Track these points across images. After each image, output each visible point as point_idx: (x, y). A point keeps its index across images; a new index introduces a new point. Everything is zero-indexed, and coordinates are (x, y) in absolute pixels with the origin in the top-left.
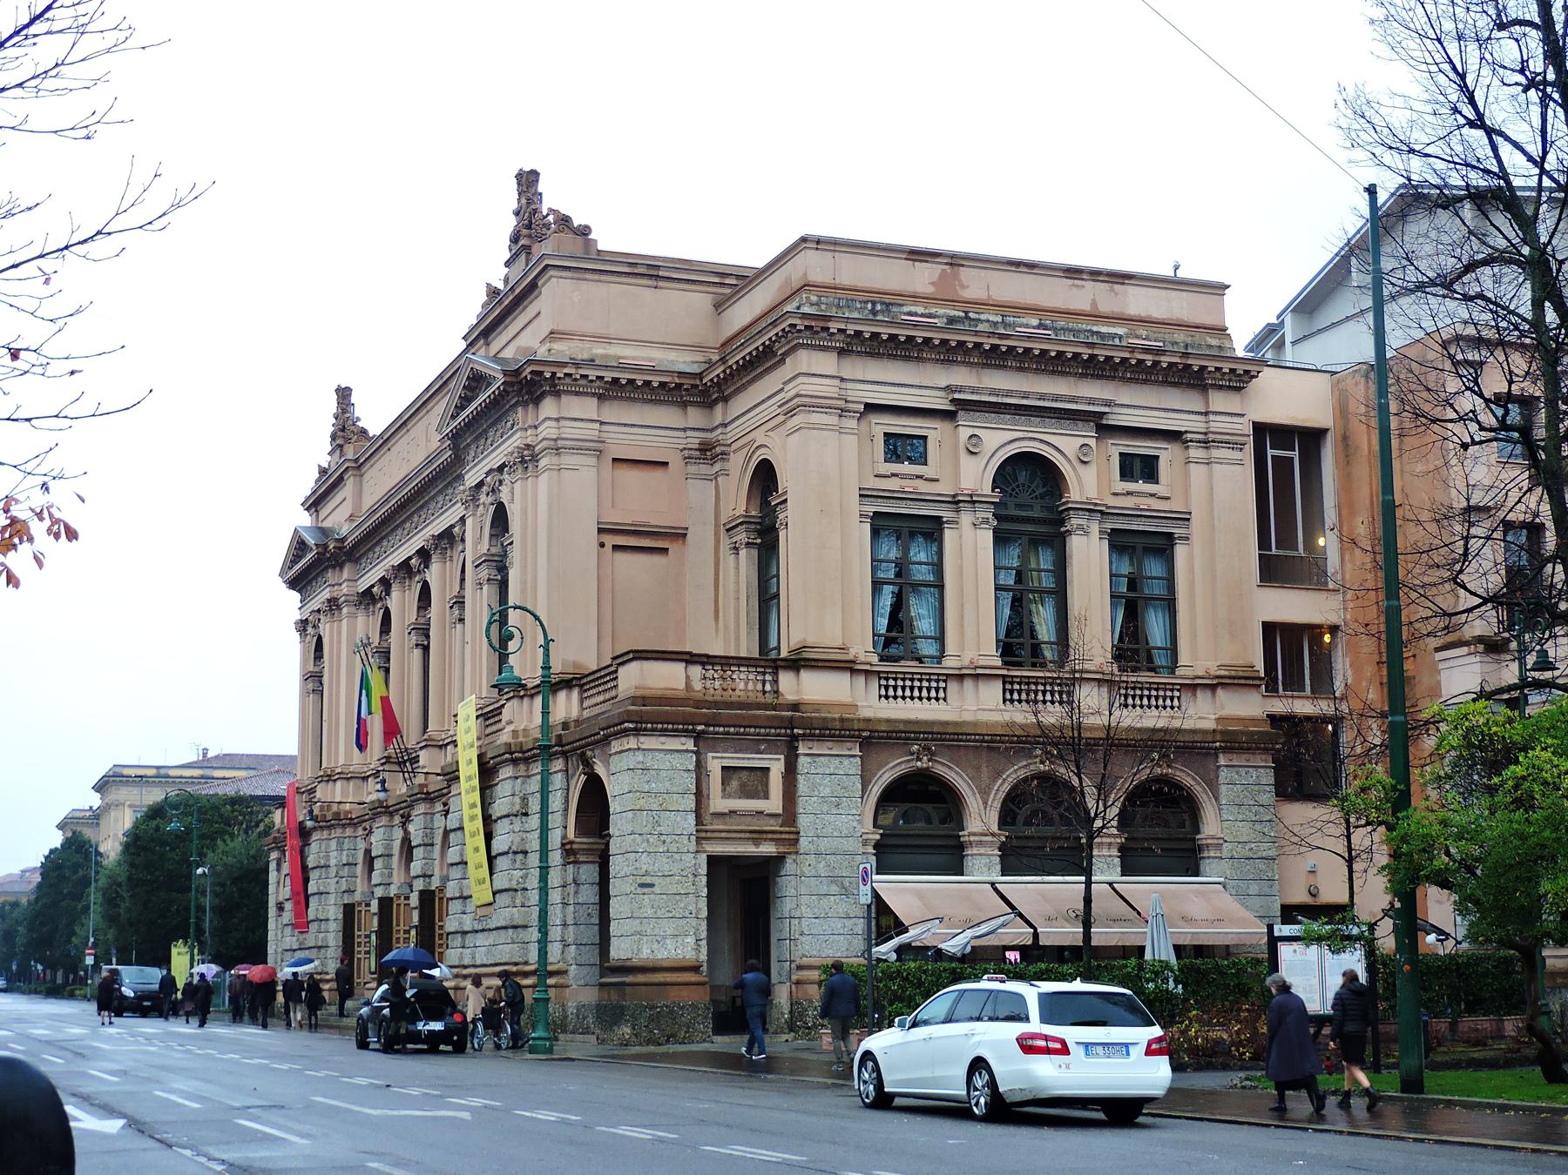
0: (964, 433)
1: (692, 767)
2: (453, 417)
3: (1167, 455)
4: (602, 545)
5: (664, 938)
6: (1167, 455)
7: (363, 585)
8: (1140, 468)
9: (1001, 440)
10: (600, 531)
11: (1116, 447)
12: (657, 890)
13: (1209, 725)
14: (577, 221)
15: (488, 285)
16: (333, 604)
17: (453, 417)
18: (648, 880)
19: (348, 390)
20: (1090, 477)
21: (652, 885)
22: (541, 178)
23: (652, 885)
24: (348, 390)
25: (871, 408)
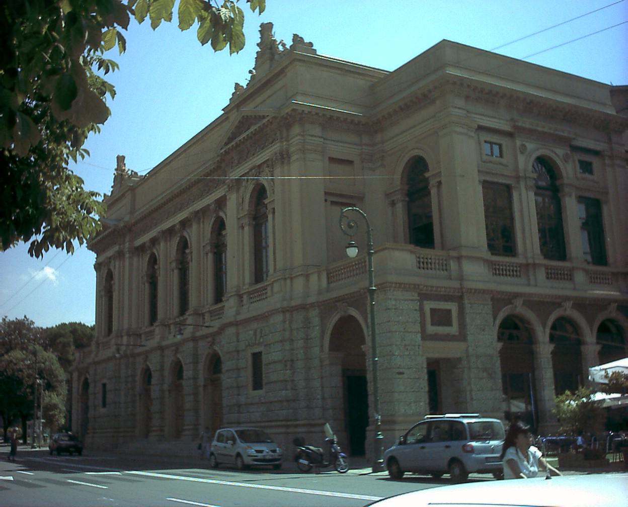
0: (518, 143)
1: (417, 308)
2: (226, 144)
3: (596, 162)
4: (326, 201)
5: (410, 403)
6: (596, 162)
7: (138, 242)
8: (586, 167)
9: (534, 149)
10: (326, 193)
11: (578, 157)
12: (405, 376)
13: (59, 364)
14: (306, 40)
15: (237, 84)
16: (120, 255)
17: (226, 144)
18: (401, 370)
19: (124, 157)
20: (569, 171)
21: (402, 373)
22: (274, 27)
23: (402, 373)
24: (124, 157)
25: (480, 128)
